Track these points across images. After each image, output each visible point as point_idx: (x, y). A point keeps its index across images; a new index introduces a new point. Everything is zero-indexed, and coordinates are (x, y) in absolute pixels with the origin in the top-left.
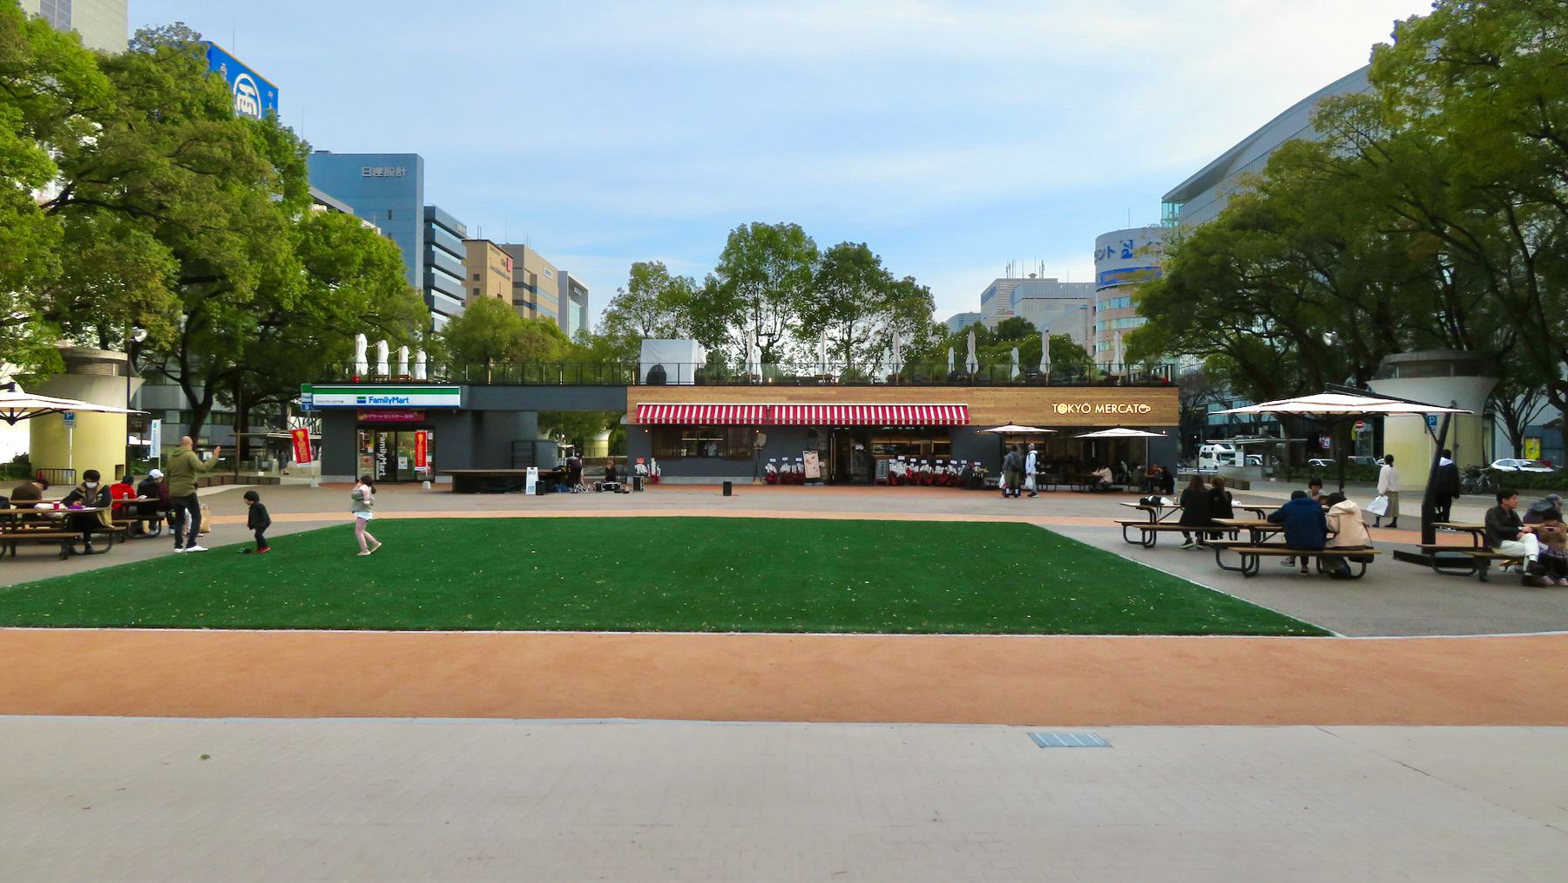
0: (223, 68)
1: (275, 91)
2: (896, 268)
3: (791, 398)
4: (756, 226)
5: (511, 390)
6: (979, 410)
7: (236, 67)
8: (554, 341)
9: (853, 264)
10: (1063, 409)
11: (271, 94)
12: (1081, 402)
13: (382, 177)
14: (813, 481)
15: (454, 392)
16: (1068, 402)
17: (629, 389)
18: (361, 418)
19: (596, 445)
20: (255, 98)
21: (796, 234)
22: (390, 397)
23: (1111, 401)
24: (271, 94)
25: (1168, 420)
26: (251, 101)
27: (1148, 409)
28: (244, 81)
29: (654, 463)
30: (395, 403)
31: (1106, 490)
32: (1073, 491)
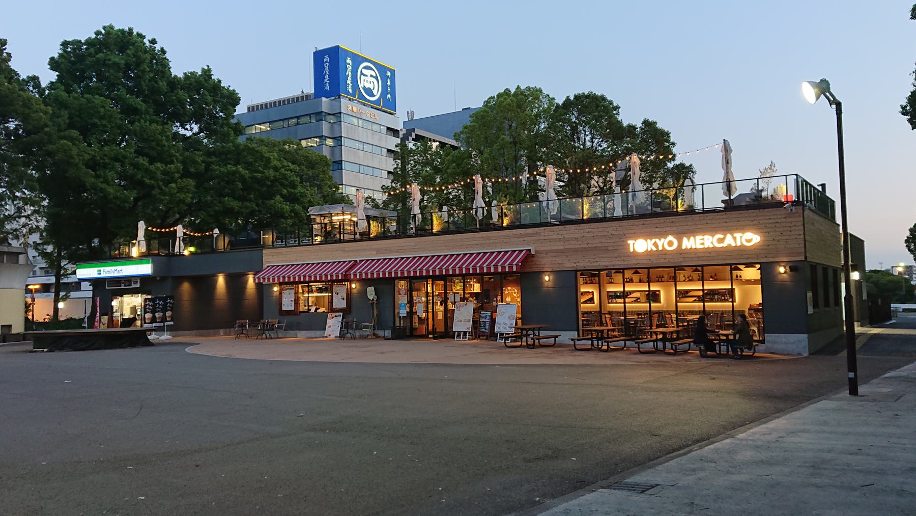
0: (349, 61)
3: (378, 251)
7: (358, 60)
11: (388, 74)
20: (376, 78)
21: (535, 94)
24: (388, 74)
28: (366, 68)
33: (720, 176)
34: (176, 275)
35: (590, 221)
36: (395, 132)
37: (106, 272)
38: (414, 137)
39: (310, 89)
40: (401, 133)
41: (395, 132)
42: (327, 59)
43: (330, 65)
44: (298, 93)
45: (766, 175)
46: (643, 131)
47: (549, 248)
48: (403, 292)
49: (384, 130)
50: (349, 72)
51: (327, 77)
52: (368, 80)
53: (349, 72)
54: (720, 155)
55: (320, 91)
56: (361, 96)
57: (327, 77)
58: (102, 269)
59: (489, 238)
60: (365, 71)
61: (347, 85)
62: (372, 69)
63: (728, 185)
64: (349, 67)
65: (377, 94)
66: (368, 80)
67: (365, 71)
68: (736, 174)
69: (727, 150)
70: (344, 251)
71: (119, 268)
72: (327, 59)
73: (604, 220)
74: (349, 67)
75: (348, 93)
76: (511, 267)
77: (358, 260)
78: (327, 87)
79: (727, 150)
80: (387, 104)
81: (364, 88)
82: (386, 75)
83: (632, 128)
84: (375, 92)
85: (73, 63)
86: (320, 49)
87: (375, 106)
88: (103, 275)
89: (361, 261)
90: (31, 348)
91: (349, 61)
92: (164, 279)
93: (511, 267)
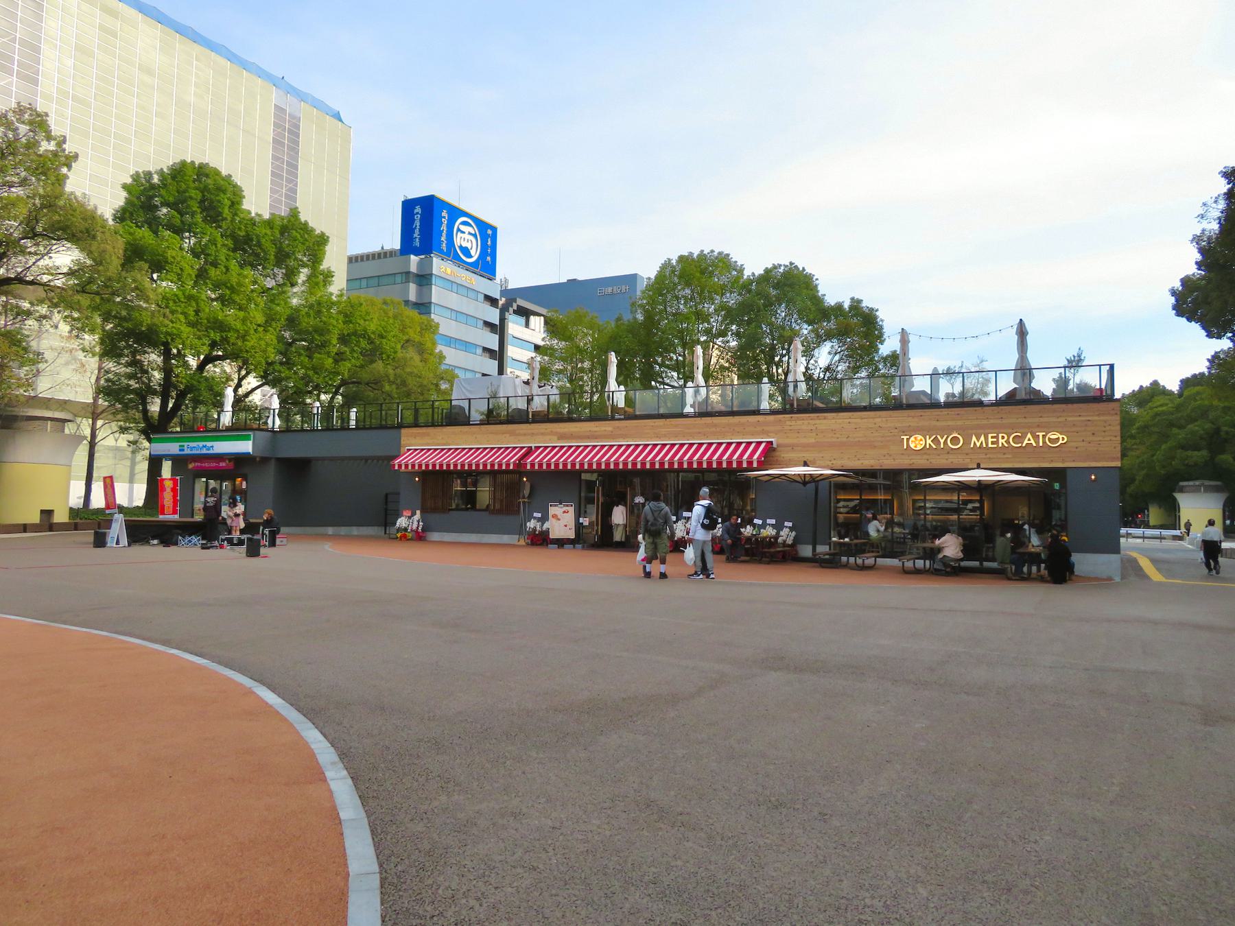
0: (444, 214)
1: (494, 229)
2: (834, 290)
3: (562, 437)
4: (681, 258)
5: (334, 433)
6: (793, 447)
7: (455, 212)
8: (362, 387)
9: (790, 286)
10: (917, 442)
11: (489, 232)
12: (946, 431)
13: (612, 294)
14: (561, 543)
15: (247, 438)
16: (925, 432)
17: (404, 431)
18: (191, 466)
19: (163, 498)
20: (475, 236)
21: (724, 262)
22: (201, 444)
23: (998, 428)
24: (489, 232)
25: (1113, 459)
26: (471, 238)
27: (1062, 439)
28: (464, 223)
29: (418, 516)
30: (204, 451)
31: (951, 571)
32: (906, 572)
33: (1012, 360)
34: (280, 456)
35: (949, 405)
36: (492, 301)
37: (192, 448)
38: (515, 307)
39: (395, 243)
40: (501, 303)
41: (492, 301)
42: (418, 209)
43: (424, 220)
44: (377, 249)
45: (1075, 363)
46: (851, 307)
47: (795, 441)
48: (168, 490)
49: (481, 297)
50: (444, 228)
51: (417, 232)
52: (465, 238)
53: (444, 228)
54: (1015, 338)
55: (407, 246)
56: (457, 257)
57: (417, 232)
58: (186, 444)
59: (715, 426)
60: (463, 228)
61: (440, 242)
62: (469, 225)
63: (1024, 371)
64: (445, 221)
65: (475, 254)
66: (465, 238)
67: (463, 228)
68: (1034, 360)
69: (1022, 332)
70: (512, 433)
71: (209, 444)
72: (418, 209)
73: (381, 427)
74: (445, 221)
75: (441, 251)
76: (508, 465)
77: (533, 445)
78: (417, 243)
79: (1022, 332)
80: (486, 266)
81: (461, 247)
82: (487, 233)
83: (839, 307)
84: (473, 252)
85: (153, 187)
86: (410, 197)
87: (472, 268)
88: (187, 452)
89: (538, 448)
90: (522, 542)
91: (444, 214)
92: (264, 460)
93: (508, 465)
